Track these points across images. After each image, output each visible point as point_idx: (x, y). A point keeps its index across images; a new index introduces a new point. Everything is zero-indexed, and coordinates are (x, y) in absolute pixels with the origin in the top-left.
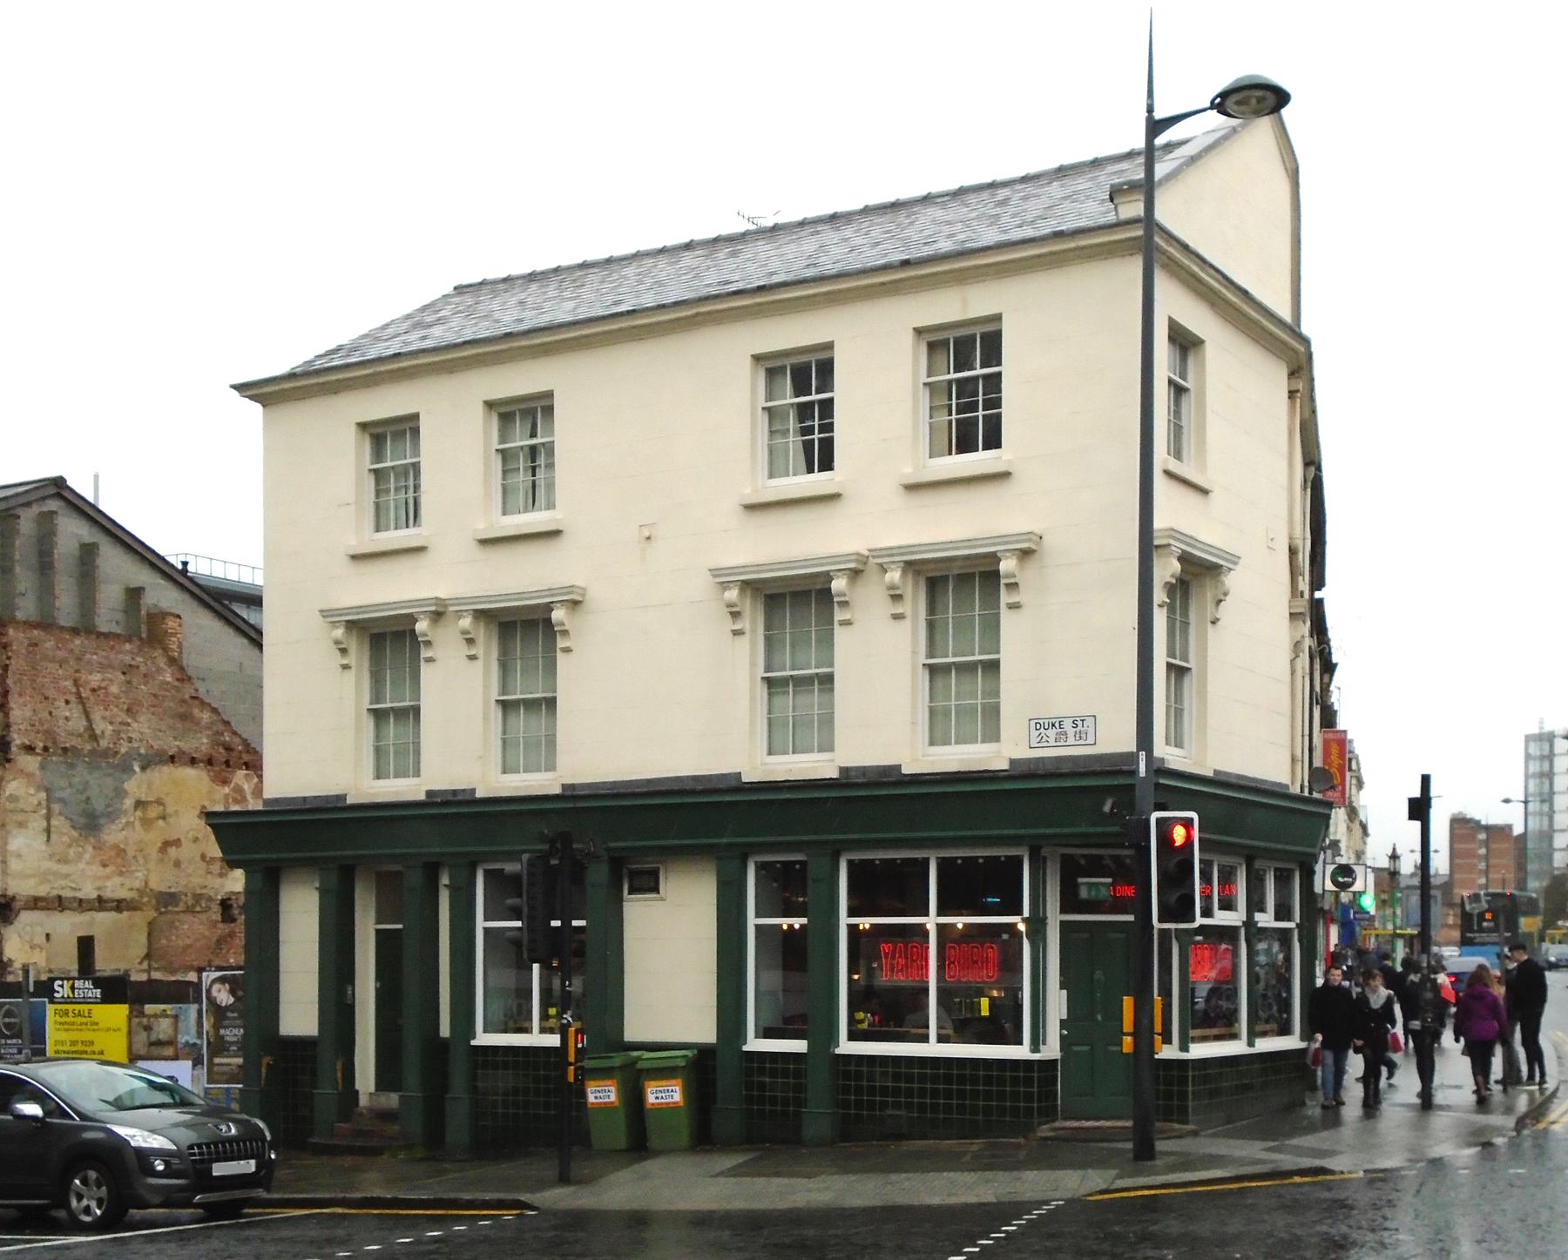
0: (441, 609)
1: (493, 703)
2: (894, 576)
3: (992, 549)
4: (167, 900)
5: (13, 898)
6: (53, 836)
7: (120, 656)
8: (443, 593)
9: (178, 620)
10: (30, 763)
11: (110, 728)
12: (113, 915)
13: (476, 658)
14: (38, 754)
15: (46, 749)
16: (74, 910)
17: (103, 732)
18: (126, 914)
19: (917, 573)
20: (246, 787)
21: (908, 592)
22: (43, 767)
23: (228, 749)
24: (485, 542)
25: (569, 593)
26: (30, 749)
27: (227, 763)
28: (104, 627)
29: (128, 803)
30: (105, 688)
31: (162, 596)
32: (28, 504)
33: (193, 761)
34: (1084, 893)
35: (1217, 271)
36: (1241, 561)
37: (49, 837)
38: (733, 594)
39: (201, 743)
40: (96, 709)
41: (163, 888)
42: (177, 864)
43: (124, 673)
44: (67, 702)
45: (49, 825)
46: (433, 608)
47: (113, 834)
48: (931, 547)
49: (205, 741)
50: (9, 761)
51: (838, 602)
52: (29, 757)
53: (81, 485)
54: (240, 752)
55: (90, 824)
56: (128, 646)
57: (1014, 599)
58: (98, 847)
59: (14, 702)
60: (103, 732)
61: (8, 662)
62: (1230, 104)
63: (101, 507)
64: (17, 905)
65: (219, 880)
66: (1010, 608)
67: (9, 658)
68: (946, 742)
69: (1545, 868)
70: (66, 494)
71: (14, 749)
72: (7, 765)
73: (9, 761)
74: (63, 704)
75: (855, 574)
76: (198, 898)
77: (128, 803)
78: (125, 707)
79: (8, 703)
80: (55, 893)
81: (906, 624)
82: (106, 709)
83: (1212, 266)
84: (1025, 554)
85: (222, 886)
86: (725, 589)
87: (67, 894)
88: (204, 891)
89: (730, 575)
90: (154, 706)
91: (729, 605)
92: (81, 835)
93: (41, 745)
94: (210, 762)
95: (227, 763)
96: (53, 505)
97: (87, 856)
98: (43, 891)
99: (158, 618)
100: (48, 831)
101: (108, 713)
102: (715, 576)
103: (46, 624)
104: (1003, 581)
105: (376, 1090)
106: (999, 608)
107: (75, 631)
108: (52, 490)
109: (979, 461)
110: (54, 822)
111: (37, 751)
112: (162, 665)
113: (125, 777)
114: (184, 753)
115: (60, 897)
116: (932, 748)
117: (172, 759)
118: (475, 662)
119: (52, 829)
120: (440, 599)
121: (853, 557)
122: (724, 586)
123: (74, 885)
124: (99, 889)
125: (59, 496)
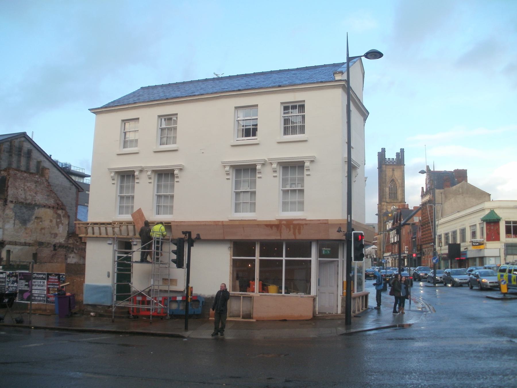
0: (142, 169)
1: (233, 192)
2: (275, 166)
3: (134, 169)
4: (41, 244)
5: (5, 241)
6: (16, 226)
7: (35, 179)
8: (143, 165)
9: (48, 170)
10: (12, 206)
11: (31, 197)
12: (28, 247)
13: (179, 182)
14: (13, 203)
15: (15, 202)
16: (19, 245)
17: (29, 198)
18: (31, 247)
19: (280, 165)
20: (61, 215)
21: (278, 170)
22: (14, 207)
23: (58, 204)
24: (279, 143)
25: (180, 166)
26: (12, 202)
27: (57, 208)
28: (32, 171)
29: (34, 217)
30: (31, 187)
31: (47, 164)
32: (17, 139)
33: (49, 207)
34: (324, 253)
35: (355, 94)
36: (360, 166)
37: (14, 226)
38: (227, 168)
39: (52, 202)
40: (28, 192)
41: (40, 241)
42: (44, 235)
43: (35, 183)
44: (21, 190)
45: (15, 222)
46: (140, 169)
47: (30, 225)
48: (125, 168)
49: (53, 202)
50: (6, 205)
51: (136, 178)
52: (11, 204)
53: (29, 134)
54: (61, 205)
55: (24, 222)
56: (37, 176)
57: (308, 173)
58: (26, 229)
59: (9, 189)
60: (29, 198)
61: (9, 179)
62: (368, 56)
63: (33, 140)
64: (6, 243)
65: (54, 239)
66: (307, 176)
67: (9, 178)
68: (123, 214)
69: (366, 249)
70: (26, 136)
71: (8, 201)
72: (6, 206)
73: (6, 205)
74: (21, 191)
75: (263, 165)
76: (49, 244)
77: (34, 217)
78: (35, 192)
79: (8, 189)
80: (14, 240)
81: (277, 179)
82: (30, 192)
83: (355, 93)
84: (312, 161)
85: (54, 241)
86: (111, 173)
87: (17, 241)
88: (50, 242)
89: (260, 161)
90: (42, 192)
91: (148, 176)
92: (22, 225)
93: (14, 201)
94: (53, 208)
95: (57, 208)
96: (23, 139)
97: (23, 231)
98: (11, 240)
99: (44, 169)
100: (14, 224)
101: (30, 193)
102: (109, 170)
103: (18, 169)
104: (257, 171)
105: (116, 300)
106: (174, 182)
107: (25, 172)
108: (23, 135)
109: (250, 140)
110: (16, 222)
111: (14, 202)
112: (44, 182)
113: (33, 211)
114: (47, 205)
115: (15, 242)
116: (120, 215)
117: (45, 206)
118: (275, 178)
119: (15, 223)
120: (142, 167)
121: (140, 167)
122: (111, 172)
123: (19, 239)
124: (25, 240)
125: (24, 137)
